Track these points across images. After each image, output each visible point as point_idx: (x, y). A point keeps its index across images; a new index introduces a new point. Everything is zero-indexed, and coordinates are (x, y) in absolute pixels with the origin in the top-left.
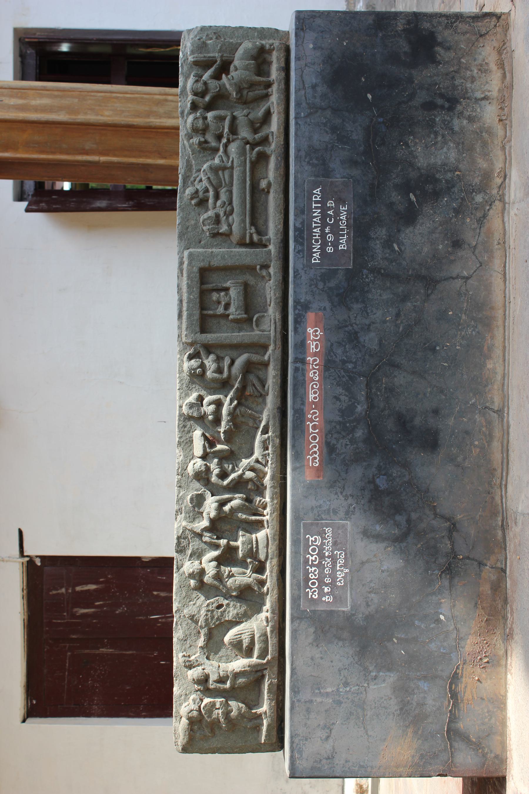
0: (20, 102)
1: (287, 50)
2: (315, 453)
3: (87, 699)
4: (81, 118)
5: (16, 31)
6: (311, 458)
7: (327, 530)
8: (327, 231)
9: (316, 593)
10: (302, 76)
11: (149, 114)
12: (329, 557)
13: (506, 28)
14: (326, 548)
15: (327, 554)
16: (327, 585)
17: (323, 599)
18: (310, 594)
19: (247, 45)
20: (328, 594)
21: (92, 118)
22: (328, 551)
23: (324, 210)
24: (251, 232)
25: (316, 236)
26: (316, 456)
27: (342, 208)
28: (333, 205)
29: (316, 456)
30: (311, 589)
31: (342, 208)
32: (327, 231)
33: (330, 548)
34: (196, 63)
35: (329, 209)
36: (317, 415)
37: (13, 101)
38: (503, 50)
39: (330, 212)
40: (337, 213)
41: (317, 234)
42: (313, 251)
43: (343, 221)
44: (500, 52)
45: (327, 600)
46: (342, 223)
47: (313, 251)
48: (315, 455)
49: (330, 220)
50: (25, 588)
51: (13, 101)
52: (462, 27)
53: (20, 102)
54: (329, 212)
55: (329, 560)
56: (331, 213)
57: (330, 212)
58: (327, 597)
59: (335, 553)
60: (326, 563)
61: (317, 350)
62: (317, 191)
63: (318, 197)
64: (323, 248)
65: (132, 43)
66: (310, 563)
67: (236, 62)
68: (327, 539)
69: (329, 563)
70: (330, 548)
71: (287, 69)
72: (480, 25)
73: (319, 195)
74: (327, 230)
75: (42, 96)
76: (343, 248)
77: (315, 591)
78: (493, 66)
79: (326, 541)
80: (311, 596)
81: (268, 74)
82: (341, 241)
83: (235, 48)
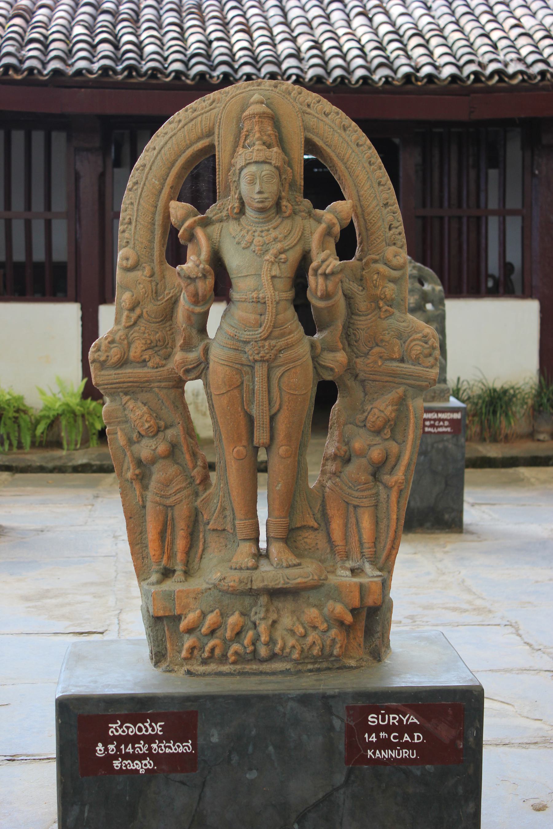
2: (147, 731)
7: (189, 744)
8: (381, 734)
14: (163, 745)
15: (154, 746)
16: (118, 748)
17: (100, 745)
18: (114, 726)
20: (106, 749)
22: (159, 747)
23: (444, 420)
26: (144, 732)
28: (416, 741)
29: (144, 732)
30: (121, 727)
33: (162, 750)
35: (412, 738)
39: (406, 738)
40: (378, 729)
42: (382, 751)
47: (382, 751)
48: (144, 729)
49: (395, 737)
50: (197, 560)
54: (406, 735)
55: (144, 750)
56: (405, 739)
57: (406, 738)
58: (102, 749)
60: (141, 746)
61: (399, 757)
65: (483, 246)
66: (380, 716)
68: (174, 745)
69: (141, 750)
70: (162, 750)
74: (383, 735)
79: (171, 745)
80: (112, 727)
82: (378, 752)
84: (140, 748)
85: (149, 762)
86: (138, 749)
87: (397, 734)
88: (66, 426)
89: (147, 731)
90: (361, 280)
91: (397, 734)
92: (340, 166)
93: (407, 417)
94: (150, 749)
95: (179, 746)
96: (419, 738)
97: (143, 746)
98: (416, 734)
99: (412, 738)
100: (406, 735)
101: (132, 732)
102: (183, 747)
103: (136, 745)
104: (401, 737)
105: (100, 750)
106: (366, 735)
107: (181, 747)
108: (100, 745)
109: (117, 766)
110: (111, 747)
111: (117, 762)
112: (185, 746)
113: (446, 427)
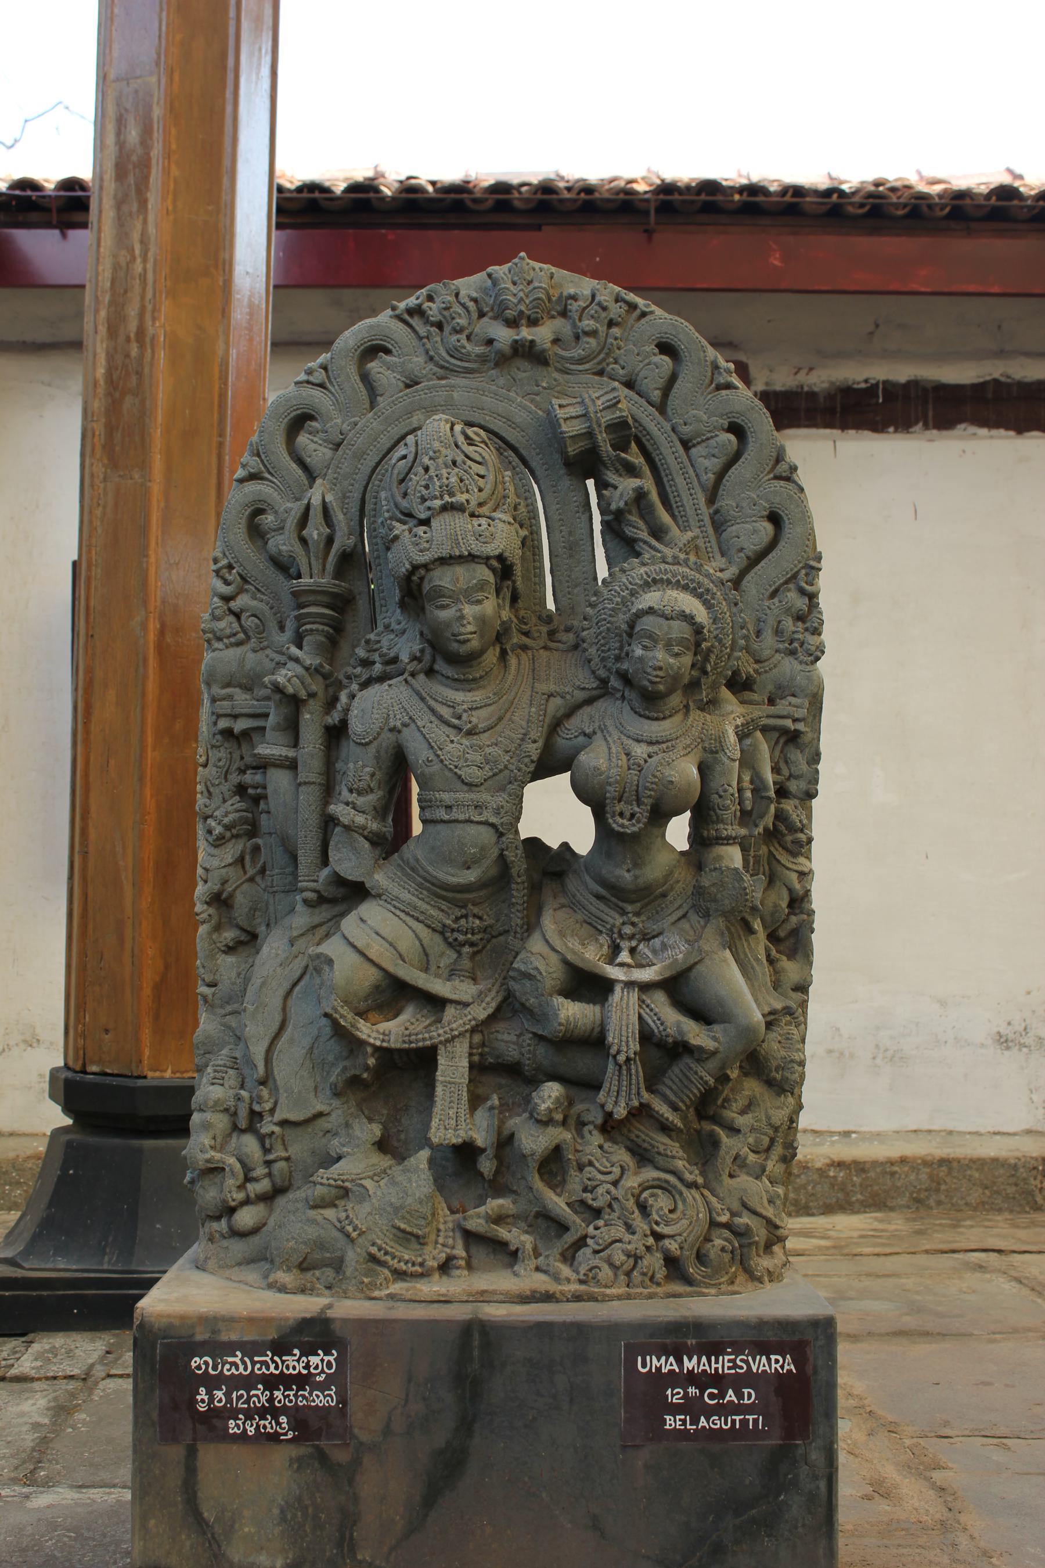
3: (878, 418)
6: (268, 1359)
7: (332, 1393)
8: (690, 1390)
9: (233, 1370)
10: (881, 1335)
12: (271, 1400)
14: (292, 1393)
16: (228, 1394)
17: (202, 1390)
23: (738, 1382)
24: (648, 1244)
25: (717, 1362)
28: (746, 1401)
32: (690, 1390)
33: (290, 1401)
35: (740, 1395)
36: (210, 1369)
39: (731, 1396)
41: (720, 1366)
42: (685, 1358)
45: (199, 1397)
49: (712, 1396)
54: (730, 1392)
56: (728, 1398)
57: (731, 1396)
58: (206, 1398)
59: (241, 1416)
60: (306, 1394)
61: (333, 1371)
62: (671, 1365)
63: (778, 1366)
64: (673, 1379)
68: (311, 1394)
73: (782, 1367)
74: (692, 1391)
76: (668, 1422)
77: (237, 1369)
84: (257, 1396)
85: (270, 1423)
86: (255, 1399)
87: (716, 1391)
88: (149, 1057)
89: (276, 1368)
90: (338, 445)
91: (716, 1391)
92: (526, 1318)
93: (549, 726)
94: (271, 1400)
95: (318, 1396)
96: (750, 1395)
98: (746, 1391)
99: (740, 1395)
100: (730, 1392)
101: (228, 1370)
102: (325, 1397)
103: (253, 1392)
104: (722, 1395)
105: (203, 1401)
106: (669, 1392)
107: (322, 1397)
108: (202, 1390)
110: (219, 1394)
112: (254, 1395)
113: (212, 1383)
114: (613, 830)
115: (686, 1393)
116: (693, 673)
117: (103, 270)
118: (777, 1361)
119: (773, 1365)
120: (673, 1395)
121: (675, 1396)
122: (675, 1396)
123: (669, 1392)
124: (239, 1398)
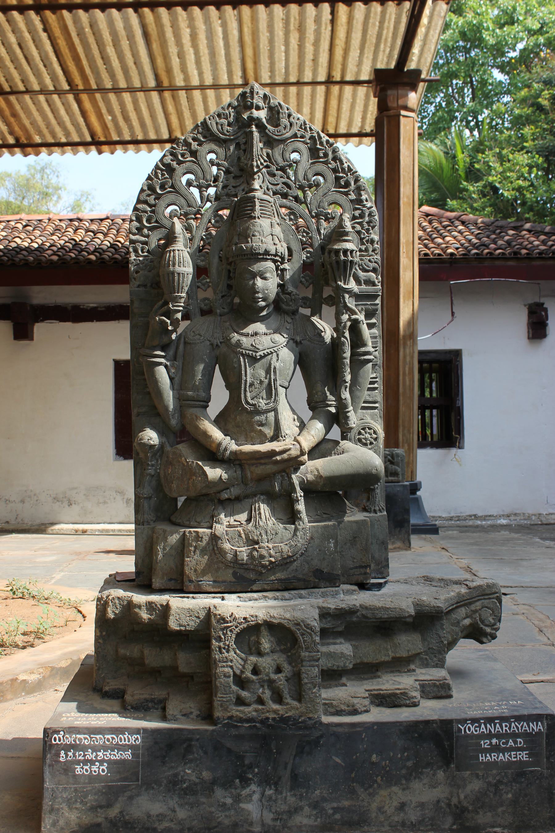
0: (407, 372)
1: (399, 482)
4: (401, 398)
5: (457, 354)
11: (404, 427)
13: (406, 550)
19: (399, 470)
21: (401, 402)
22: (104, 755)
23: (514, 736)
27: (526, 754)
31: (526, 754)
34: (393, 454)
35: (515, 742)
37: (407, 369)
38: (399, 549)
43: (478, 729)
44: (399, 548)
46: (476, 727)
49: (503, 743)
51: (407, 369)
52: (406, 536)
53: (407, 372)
57: (511, 743)
64: (483, 736)
67: (394, 467)
71: (392, 482)
72: (407, 542)
75: (410, 381)
78: (394, 546)
81: (391, 476)
83: (398, 466)
95: (121, 754)
97: (92, 754)
104: (507, 743)
109: (95, 772)
110: (70, 754)
111: (79, 767)
114: (219, 138)
115: (491, 743)
116: (201, 295)
117: (172, 767)
118: (506, 726)
119: (504, 728)
120: (484, 744)
121: (485, 743)
122: (485, 743)
123: (482, 742)
124: (80, 755)
